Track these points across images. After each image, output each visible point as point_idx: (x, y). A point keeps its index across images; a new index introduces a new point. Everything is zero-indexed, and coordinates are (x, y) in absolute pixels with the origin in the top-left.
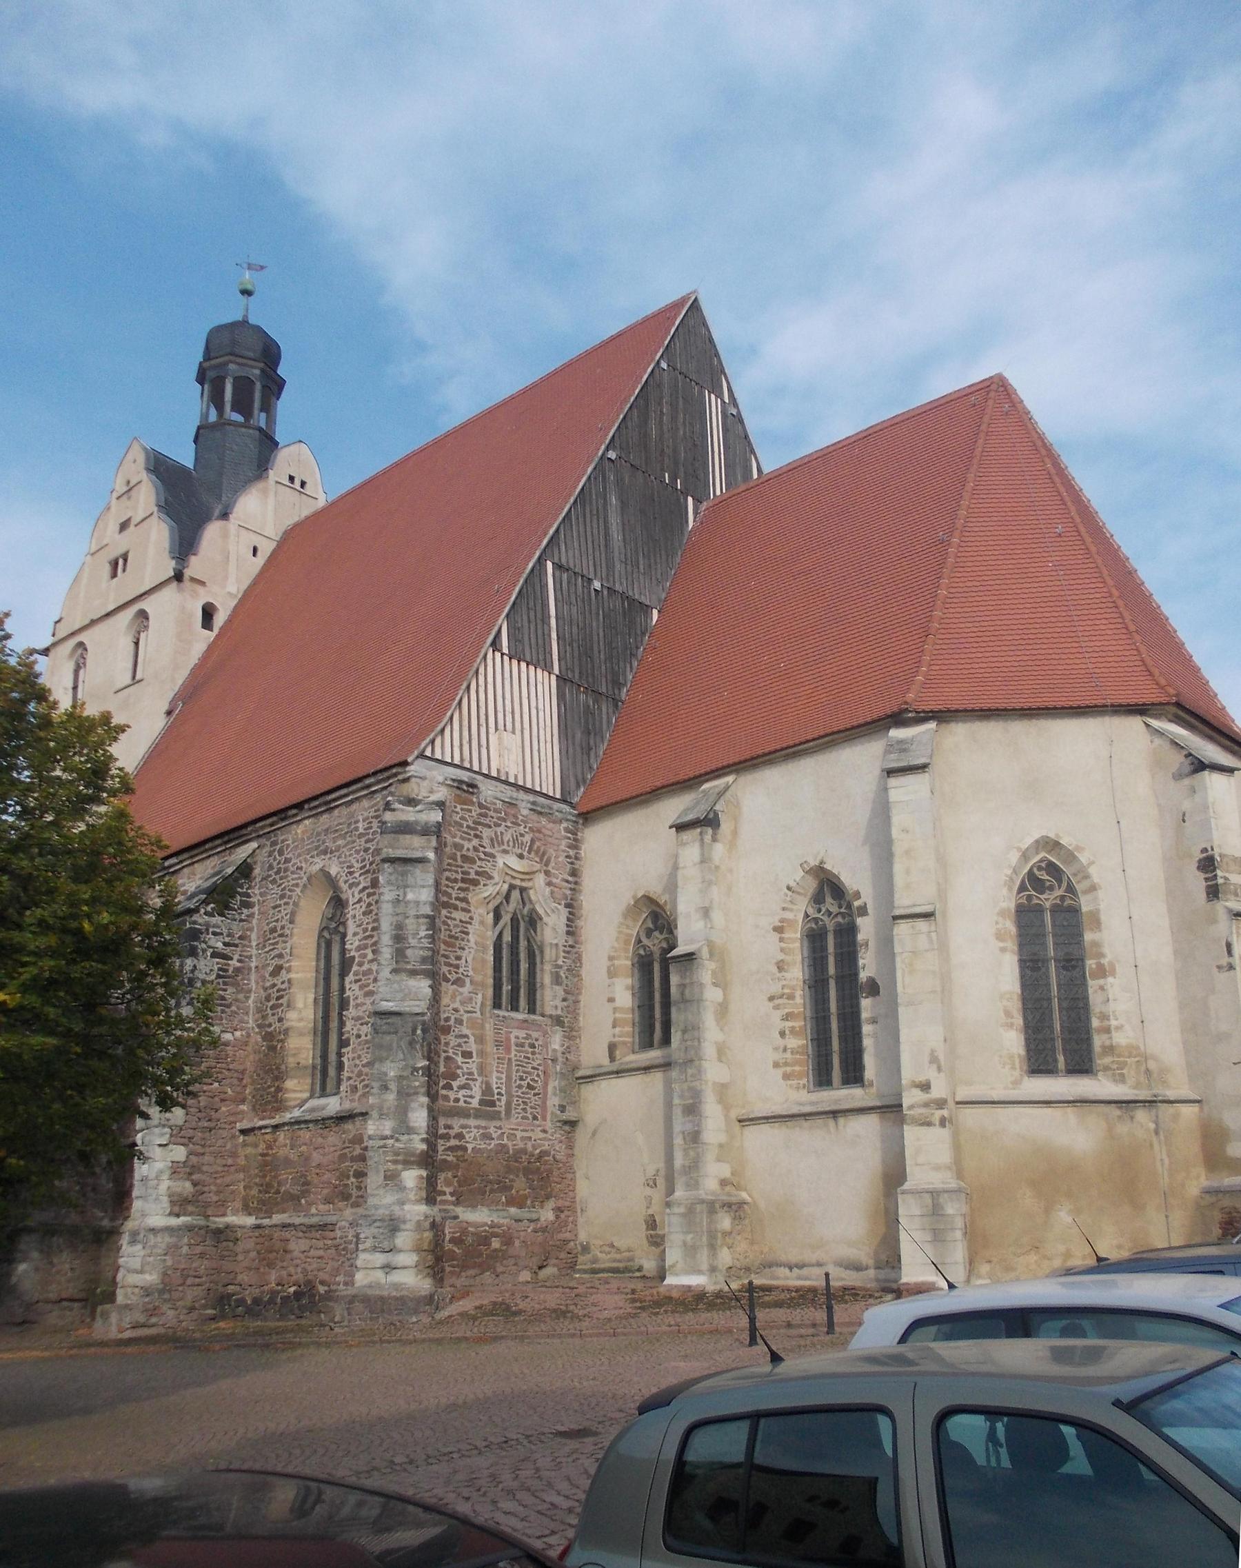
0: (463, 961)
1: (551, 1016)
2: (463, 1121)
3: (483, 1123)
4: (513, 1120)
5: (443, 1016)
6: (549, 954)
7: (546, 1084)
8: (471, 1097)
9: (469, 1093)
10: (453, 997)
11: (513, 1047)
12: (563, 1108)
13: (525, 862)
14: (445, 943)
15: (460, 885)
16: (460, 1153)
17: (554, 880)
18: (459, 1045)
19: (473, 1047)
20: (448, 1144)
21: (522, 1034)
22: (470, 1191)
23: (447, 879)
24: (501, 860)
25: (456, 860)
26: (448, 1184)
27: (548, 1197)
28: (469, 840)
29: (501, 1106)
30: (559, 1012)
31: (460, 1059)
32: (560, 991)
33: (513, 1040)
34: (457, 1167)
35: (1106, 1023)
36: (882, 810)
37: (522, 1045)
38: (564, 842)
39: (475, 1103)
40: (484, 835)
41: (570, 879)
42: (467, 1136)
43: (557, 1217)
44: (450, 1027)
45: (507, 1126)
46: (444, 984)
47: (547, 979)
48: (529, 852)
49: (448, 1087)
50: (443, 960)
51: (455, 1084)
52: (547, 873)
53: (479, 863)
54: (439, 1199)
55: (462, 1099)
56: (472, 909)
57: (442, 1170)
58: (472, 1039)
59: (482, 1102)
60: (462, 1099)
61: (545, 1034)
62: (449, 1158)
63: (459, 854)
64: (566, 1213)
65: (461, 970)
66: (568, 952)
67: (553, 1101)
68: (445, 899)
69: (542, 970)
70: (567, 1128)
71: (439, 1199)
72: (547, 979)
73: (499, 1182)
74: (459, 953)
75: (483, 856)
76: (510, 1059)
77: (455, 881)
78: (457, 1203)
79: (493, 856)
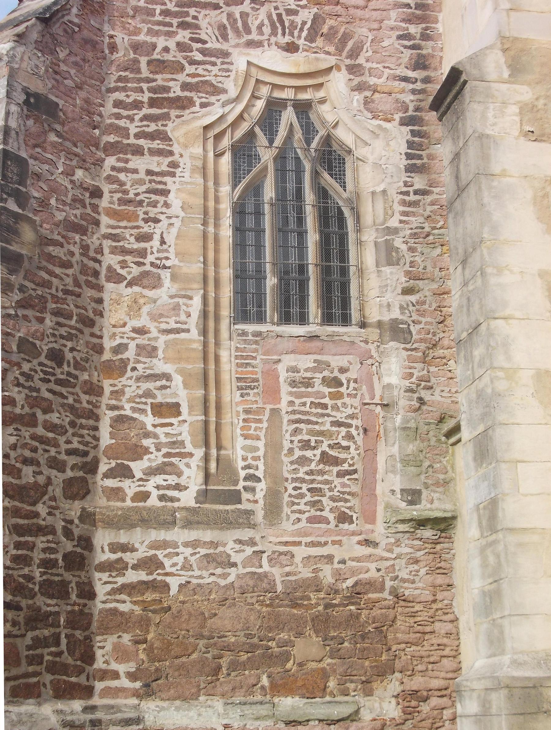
0: (156, 243)
1: (380, 324)
2: (155, 535)
3: (208, 535)
4: (287, 526)
5: (108, 344)
6: (371, 212)
7: (370, 454)
8: (178, 487)
9: (172, 480)
10: (135, 308)
11: (285, 389)
12: (413, 496)
13: (299, 56)
14: (112, 213)
15: (146, 111)
16: (149, 596)
17: (373, 81)
18: (148, 394)
19: (180, 392)
20: (121, 581)
21: (306, 362)
22: (181, 667)
23: (118, 104)
24: (240, 61)
25: (139, 71)
26: (121, 654)
27: (383, 671)
28: (169, 34)
29: (256, 500)
30: (396, 314)
31: (149, 420)
32: (395, 276)
33: (283, 375)
34: (144, 623)
35: (99, 257)
36: (522, 495)
37: (308, 383)
38: (393, 14)
39: (187, 499)
40: (203, 23)
41: (411, 74)
42: (167, 563)
43: (409, 713)
44: (124, 363)
45: (270, 539)
46: (109, 286)
47: (369, 258)
48: (311, 38)
49: (125, 472)
50: (107, 244)
51: (138, 467)
52: (353, 69)
53: (190, 70)
54: (99, 686)
55: (155, 493)
56: (176, 148)
57: (106, 630)
58: (178, 380)
59: (204, 496)
60: (155, 493)
61: (365, 358)
62: (124, 608)
63: (143, 61)
64: (434, 701)
65: (150, 258)
66: (415, 204)
67: (389, 484)
68: (112, 138)
69: (360, 243)
70: (428, 533)
71: (99, 686)
72: (369, 258)
73: (252, 648)
74: (146, 229)
75: (199, 57)
76: (275, 412)
77: (137, 105)
78: (148, 692)
79: (226, 54)
